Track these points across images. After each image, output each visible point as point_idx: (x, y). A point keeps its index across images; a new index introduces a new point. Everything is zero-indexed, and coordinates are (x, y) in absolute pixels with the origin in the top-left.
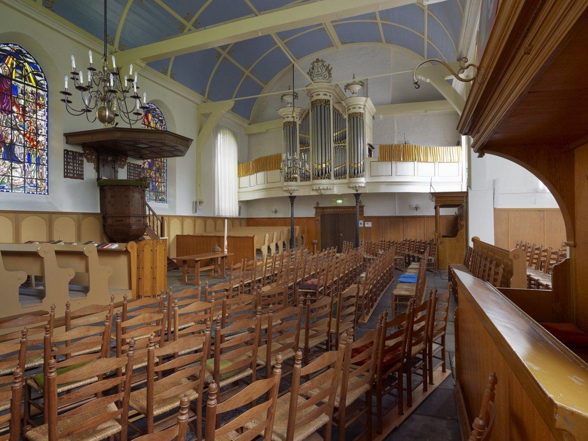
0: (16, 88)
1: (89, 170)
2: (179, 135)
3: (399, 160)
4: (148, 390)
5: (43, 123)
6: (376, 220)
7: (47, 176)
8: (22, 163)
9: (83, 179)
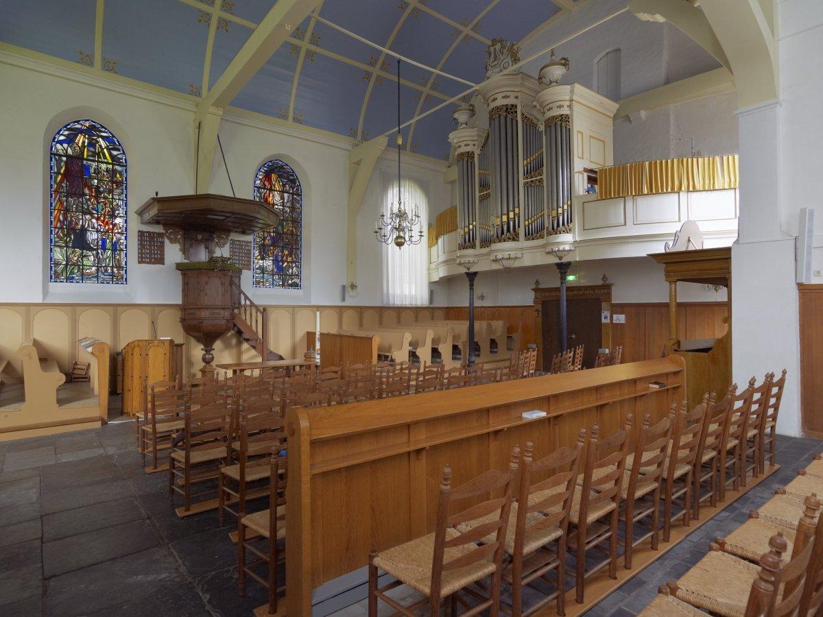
0: (88, 168)
1: (173, 253)
2: (245, 200)
3: (640, 193)
4: (244, 536)
5: (120, 203)
6: (636, 310)
7: (126, 262)
8: (95, 250)
9: (163, 264)
